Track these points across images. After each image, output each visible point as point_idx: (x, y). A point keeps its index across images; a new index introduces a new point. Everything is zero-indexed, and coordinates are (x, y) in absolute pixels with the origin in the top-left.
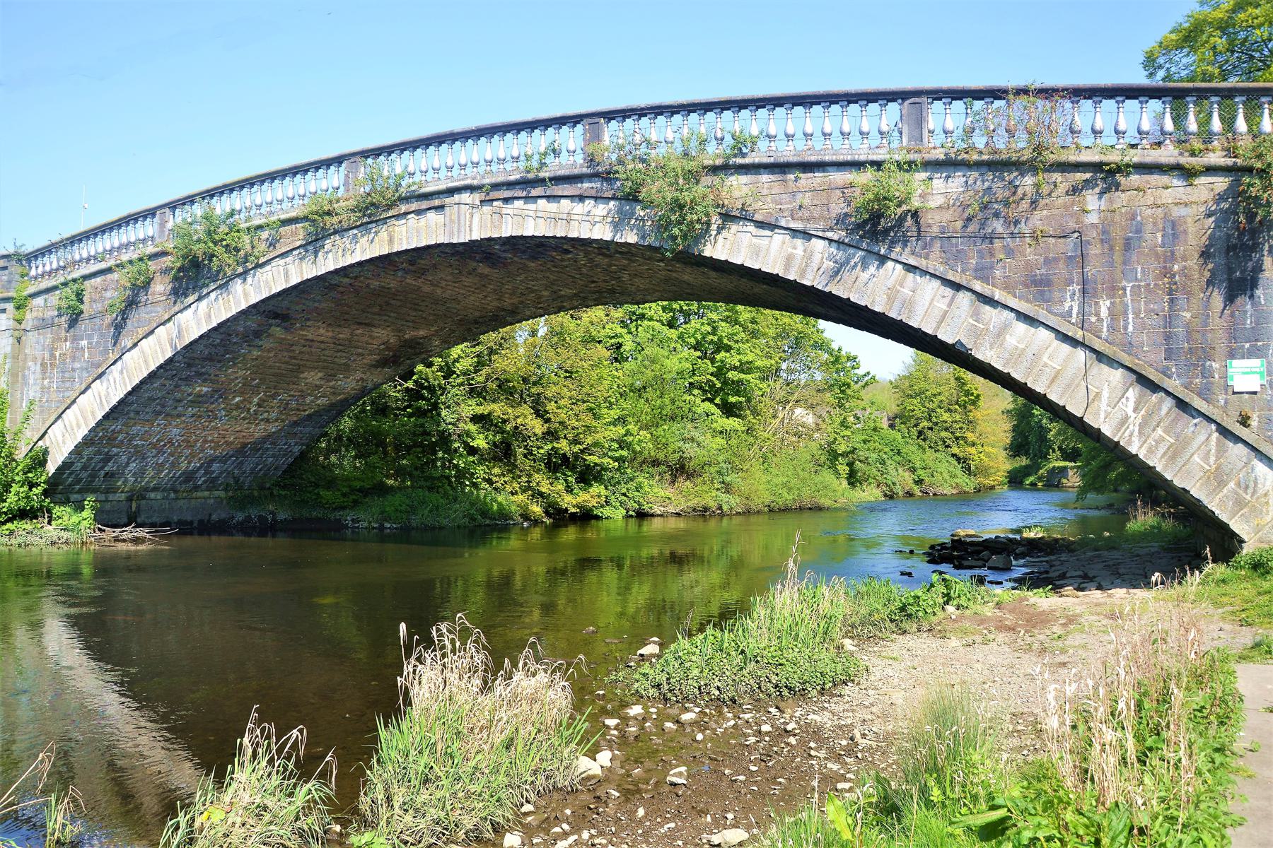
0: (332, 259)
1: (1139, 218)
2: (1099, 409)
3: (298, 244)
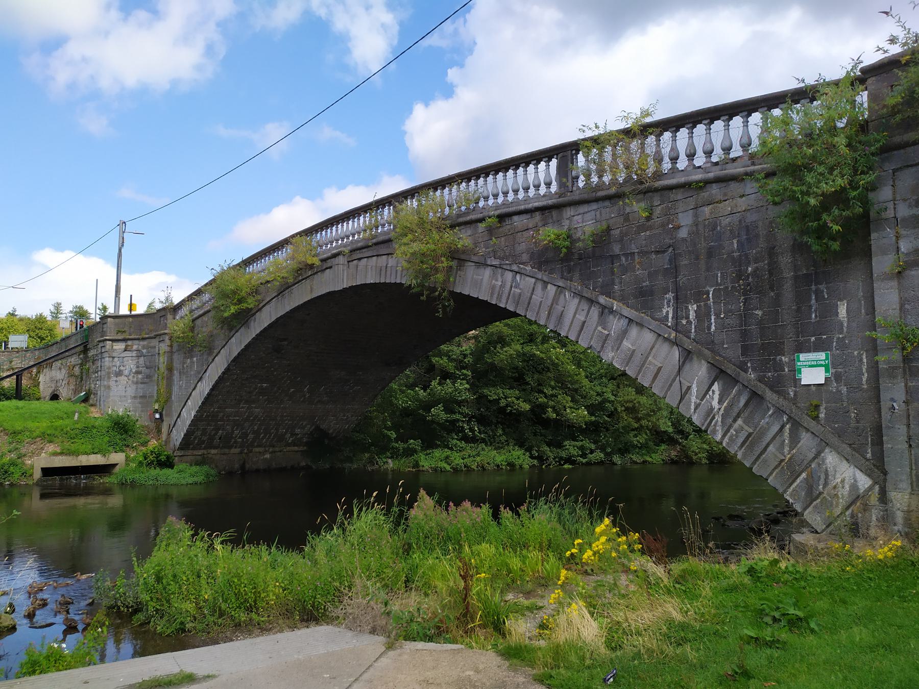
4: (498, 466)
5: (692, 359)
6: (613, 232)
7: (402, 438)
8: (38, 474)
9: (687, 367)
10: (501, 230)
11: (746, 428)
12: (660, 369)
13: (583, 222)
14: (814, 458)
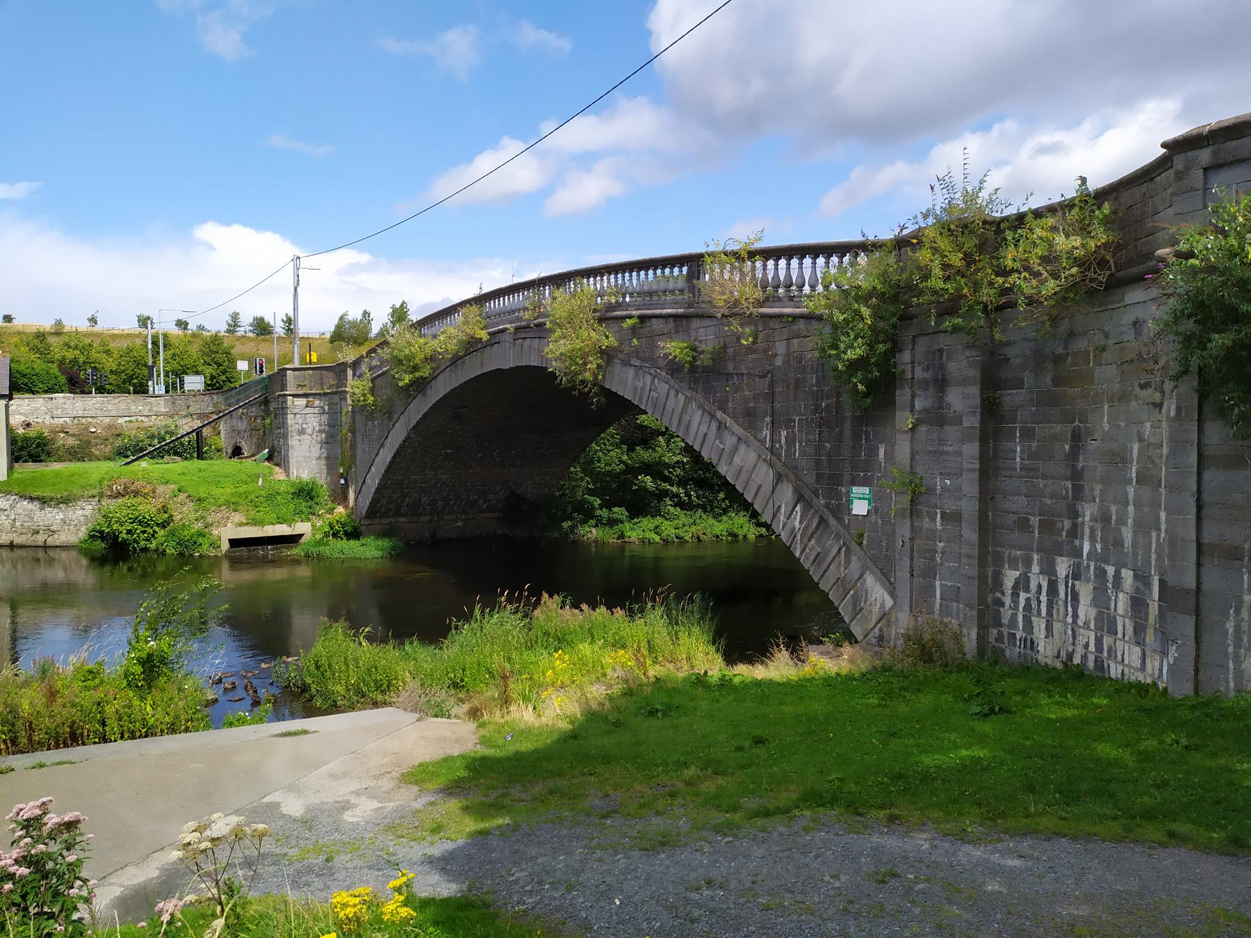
4: (717, 537)
5: (782, 481)
6: (728, 350)
7: (607, 505)
8: (225, 546)
9: (779, 487)
10: (642, 330)
11: (817, 547)
12: (760, 486)
13: (706, 336)
14: (859, 578)
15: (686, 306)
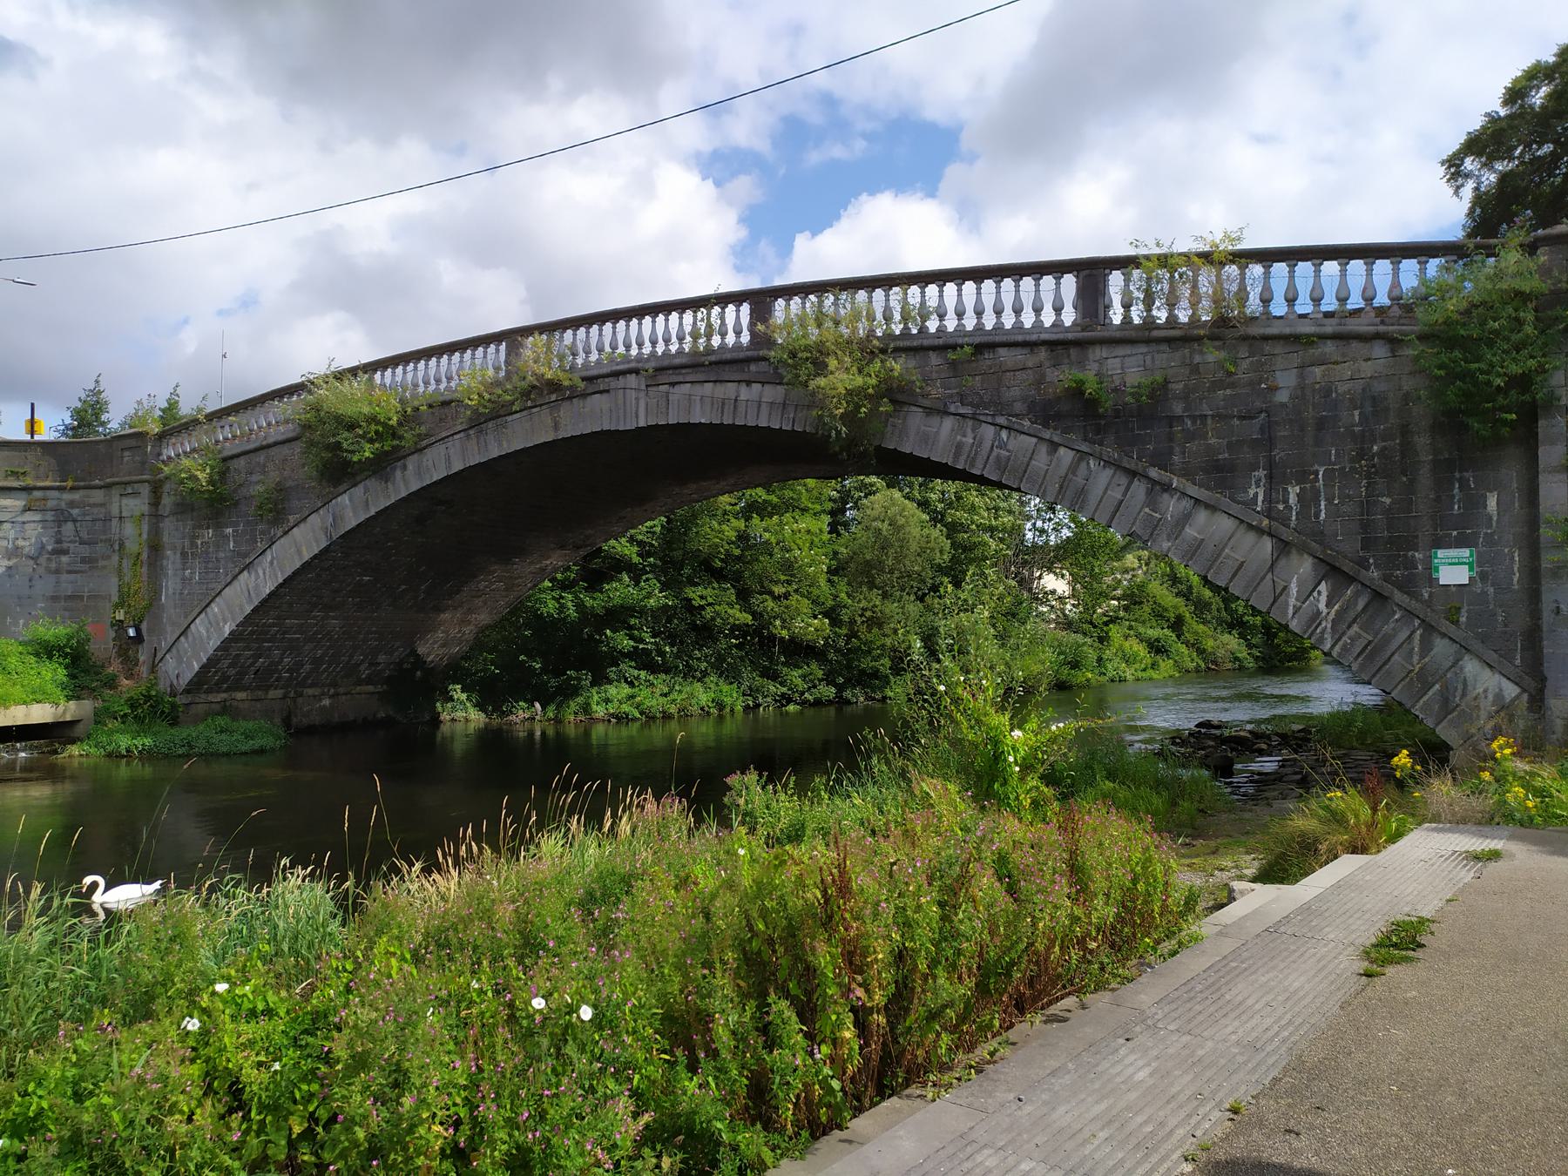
0: (496, 446)
1: (1334, 395)
2: (1287, 604)
3: (459, 428)
15: (1079, 329)
